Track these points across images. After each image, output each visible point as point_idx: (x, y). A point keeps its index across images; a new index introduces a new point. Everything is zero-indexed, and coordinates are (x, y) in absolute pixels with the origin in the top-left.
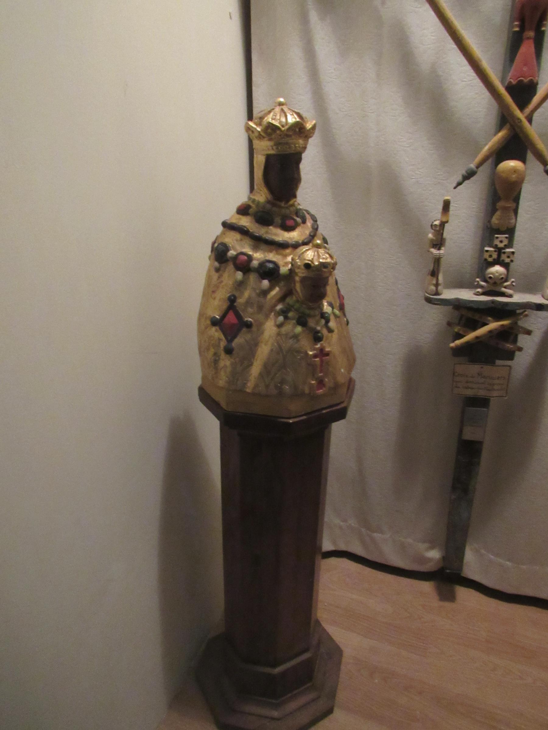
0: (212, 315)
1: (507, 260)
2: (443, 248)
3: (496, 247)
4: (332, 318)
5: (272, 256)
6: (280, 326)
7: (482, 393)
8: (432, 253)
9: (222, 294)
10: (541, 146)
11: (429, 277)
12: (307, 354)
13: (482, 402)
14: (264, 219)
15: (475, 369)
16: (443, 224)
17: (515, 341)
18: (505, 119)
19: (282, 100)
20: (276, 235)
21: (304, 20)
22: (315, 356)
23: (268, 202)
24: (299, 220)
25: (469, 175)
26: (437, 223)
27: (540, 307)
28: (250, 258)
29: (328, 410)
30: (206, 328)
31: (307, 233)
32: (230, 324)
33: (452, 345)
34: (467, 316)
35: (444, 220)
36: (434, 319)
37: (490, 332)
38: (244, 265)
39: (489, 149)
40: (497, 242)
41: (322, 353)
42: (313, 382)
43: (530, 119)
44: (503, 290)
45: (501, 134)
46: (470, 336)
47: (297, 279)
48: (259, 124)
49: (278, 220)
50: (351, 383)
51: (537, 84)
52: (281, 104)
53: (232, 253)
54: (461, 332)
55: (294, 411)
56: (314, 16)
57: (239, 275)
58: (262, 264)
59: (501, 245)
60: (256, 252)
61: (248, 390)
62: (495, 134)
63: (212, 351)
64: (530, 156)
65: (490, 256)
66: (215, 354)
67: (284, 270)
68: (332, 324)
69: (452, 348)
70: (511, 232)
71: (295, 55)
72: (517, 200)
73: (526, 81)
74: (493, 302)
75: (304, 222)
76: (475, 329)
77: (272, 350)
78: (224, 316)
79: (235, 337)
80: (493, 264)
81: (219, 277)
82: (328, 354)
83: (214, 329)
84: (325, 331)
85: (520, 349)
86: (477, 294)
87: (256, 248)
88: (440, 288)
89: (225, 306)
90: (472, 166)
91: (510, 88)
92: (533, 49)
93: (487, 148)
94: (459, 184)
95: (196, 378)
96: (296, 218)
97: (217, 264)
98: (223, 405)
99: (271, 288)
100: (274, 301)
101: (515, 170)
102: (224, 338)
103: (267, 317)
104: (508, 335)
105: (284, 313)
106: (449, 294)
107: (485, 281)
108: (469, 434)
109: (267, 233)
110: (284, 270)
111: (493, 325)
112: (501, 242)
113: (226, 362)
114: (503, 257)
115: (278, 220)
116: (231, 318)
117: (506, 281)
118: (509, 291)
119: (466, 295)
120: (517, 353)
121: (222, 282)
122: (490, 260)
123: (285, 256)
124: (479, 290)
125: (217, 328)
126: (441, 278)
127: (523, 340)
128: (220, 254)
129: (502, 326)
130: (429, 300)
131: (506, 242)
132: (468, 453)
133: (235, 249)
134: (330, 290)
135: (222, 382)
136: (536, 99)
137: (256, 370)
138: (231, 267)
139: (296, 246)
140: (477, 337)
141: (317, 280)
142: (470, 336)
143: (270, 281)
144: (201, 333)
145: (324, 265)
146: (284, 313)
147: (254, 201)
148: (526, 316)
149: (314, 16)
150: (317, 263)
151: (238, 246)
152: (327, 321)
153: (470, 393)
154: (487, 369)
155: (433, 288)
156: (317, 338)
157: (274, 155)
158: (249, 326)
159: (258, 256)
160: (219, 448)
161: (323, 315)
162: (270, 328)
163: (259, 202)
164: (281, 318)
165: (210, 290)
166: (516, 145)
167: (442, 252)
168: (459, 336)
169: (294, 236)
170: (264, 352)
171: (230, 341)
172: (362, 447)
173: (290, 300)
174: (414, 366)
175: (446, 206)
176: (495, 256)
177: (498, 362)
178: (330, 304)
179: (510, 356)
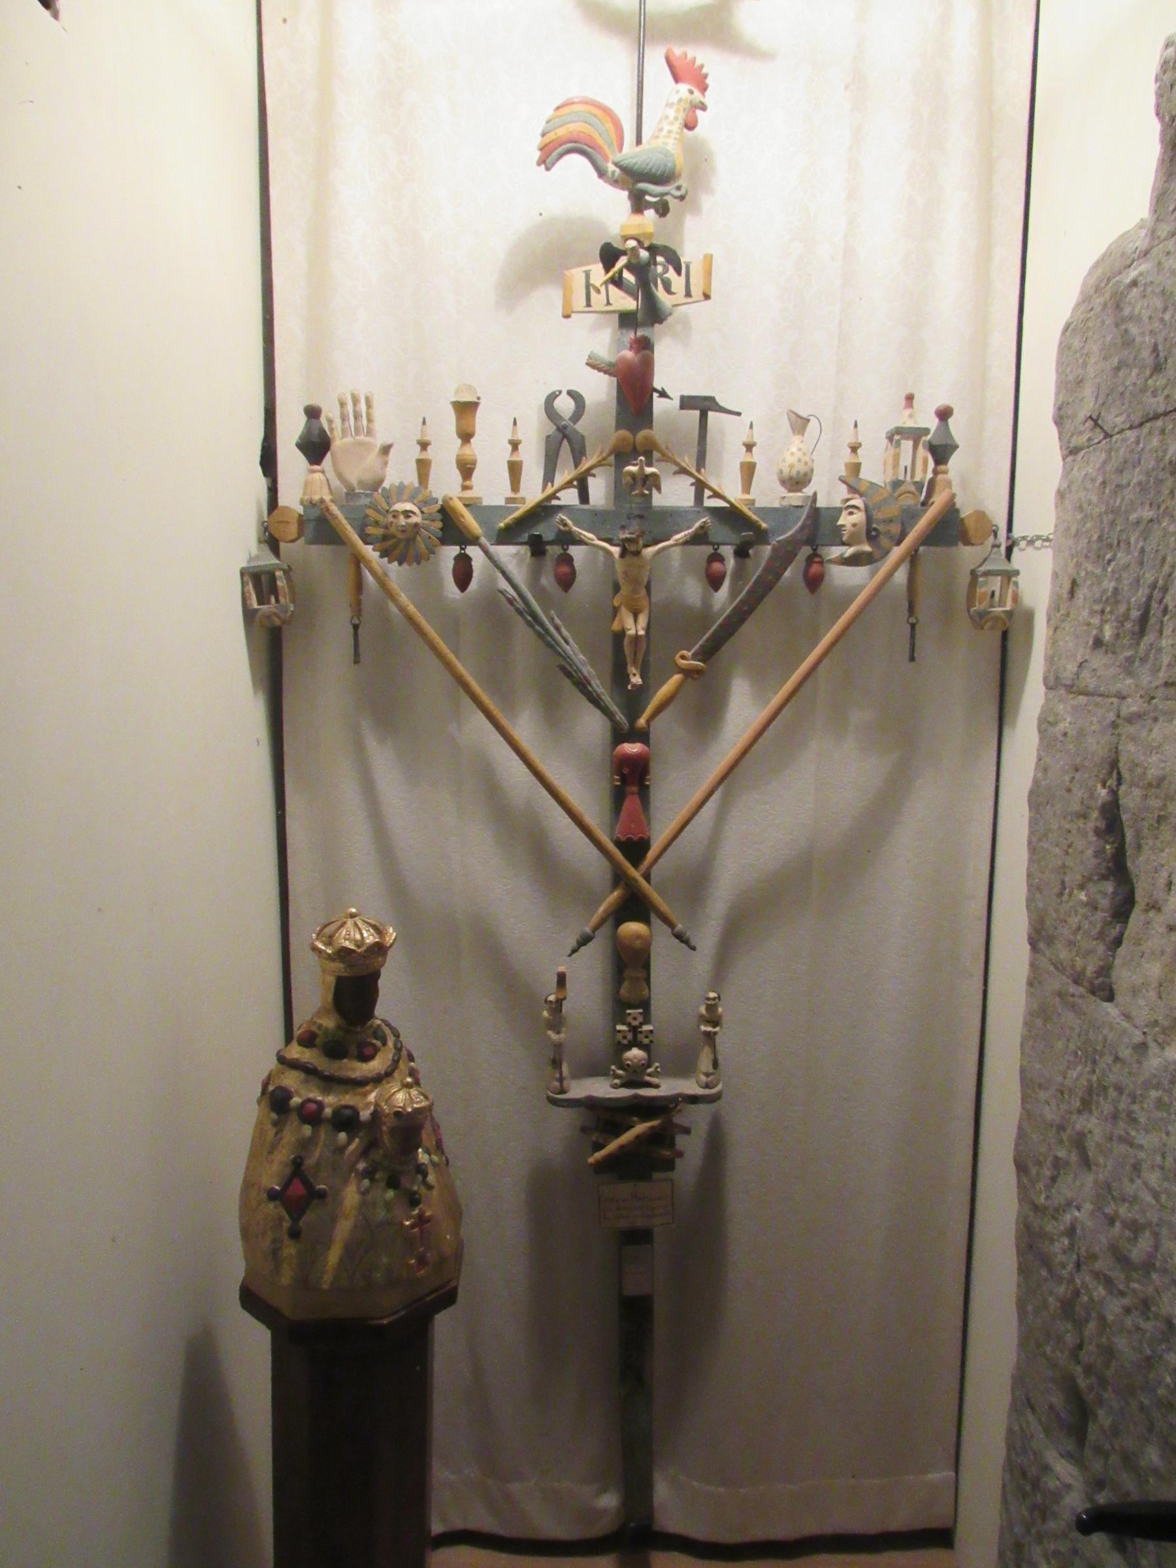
0: (270, 1186)
1: (646, 1041)
2: (564, 1029)
3: (629, 1025)
4: (430, 1170)
5: (348, 1099)
6: (364, 1193)
7: (640, 1223)
8: (549, 1038)
9: (284, 1155)
10: (664, 907)
11: (550, 1068)
12: (402, 1224)
13: (638, 1237)
14: (335, 1050)
15: (625, 1189)
16: (559, 1002)
17: (672, 1144)
18: (618, 877)
19: (354, 910)
20: (353, 1070)
21: (359, 748)
22: (412, 1226)
23: (339, 1027)
24: (378, 1043)
25: (585, 940)
26: (552, 998)
27: (694, 1099)
28: (321, 1106)
29: (433, 1296)
30: (259, 1204)
31: (390, 1056)
32: (296, 1197)
33: (591, 1160)
34: (605, 1118)
35: (561, 997)
36: (561, 1126)
37: (638, 1137)
38: (311, 1116)
39: (604, 911)
40: (629, 1019)
41: (421, 1220)
42: (413, 1261)
43: (647, 877)
44: (648, 1078)
45: (616, 894)
46: (613, 1146)
47: (385, 1128)
48: (329, 943)
49: (353, 1049)
50: (460, 1245)
51: (649, 838)
52: (352, 916)
53: (296, 1100)
54: (601, 1141)
55: (387, 1308)
56: (372, 744)
57: (307, 1130)
58: (337, 1112)
59: (635, 1023)
60: (328, 1094)
61: (325, 1287)
62: (612, 892)
63: (270, 1236)
64: (654, 918)
65: (625, 1037)
66: (274, 1241)
67: (365, 1115)
68: (431, 1178)
69: (591, 1165)
70: (645, 1005)
71: (349, 791)
72: (647, 966)
73: (635, 838)
74: (636, 1097)
75: (385, 1044)
76: (618, 1135)
77: (355, 1226)
78: (286, 1185)
79: (302, 1213)
80: (629, 1047)
81: (277, 1134)
82: (428, 1220)
83: (271, 1205)
84: (423, 1190)
85: (680, 1154)
86: (615, 1086)
87: (326, 1091)
88: (565, 1083)
89: (288, 1171)
90: (588, 930)
91: (618, 843)
92: (638, 801)
93: (602, 909)
94: (574, 951)
95: (235, 1269)
96: (374, 1041)
97: (274, 1116)
98: (287, 1311)
99: (349, 1142)
100: (353, 1159)
101: (638, 936)
102: (287, 1217)
103: (346, 1182)
104: (662, 1138)
105: (369, 1174)
106: (580, 1089)
107: (621, 1068)
108: (632, 1289)
109: (340, 1068)
110: (365, 1115)
111: (640, 1128)
112: (635, 1019)
113: (290, 1249)
114: (640, 1037)
115: (353, 1049)
116: (297, 1189)
117: (649, 1066)
118: (654, 1080)
119: (602, 1088)
120: (678, 1161)
121: (281, 1139)
122: (625, 1042)
123: (366, 1095)
124: (617, 1081)
125: (278, 1203)
126: (565, 1068)
127: (681, 1141)
128: (277, 1101)
129: (652, 1128)
130: (554, 1102)
131: (640, 1019)
132: (635, 1314)
133: (300, 1096)
134: (426, 1135)
135: (286, 1277)
136: (651, 855)
137: (334, 1256)
138: (294, 1119)
139: (377, 1080)
140: (622, 1147)
141: (410, 1129)
142: (613, 1146)
143: (348, 1133)
144: (246, 1207)
145: (417, 1111)
146: (369, 1174)
147: (320, 1027)
148: (680, 1111)
149: (372, 744)
150: (410, 1110)
151: (303, 1092)
152: (425, 1175)
153: (623, 1224)
154: (643, 1187)
155: (557, 1084)
156: (413, 1200)
157: (347, 978)
158: (322, 1195)
159: (331, 1101)
160: (268, 1374)
161: (421, 1170)
162: (351, 1195)
163: (327, 1029)
164: (366, 1182)
165: (260, 1150)
166: (634, 905)
167: (562, 1035)
168: (598, 1147)
169: (376, 1065)
170: (343, 1229)
171: (295, 1219)
172: (481, 1348)
173: (376, 1155)
174: (544, 1190)
175: (562, 979)
176: (630, 1036)
177: (656, 1175)
178: (427, 1151)
179: (669, 1165)
